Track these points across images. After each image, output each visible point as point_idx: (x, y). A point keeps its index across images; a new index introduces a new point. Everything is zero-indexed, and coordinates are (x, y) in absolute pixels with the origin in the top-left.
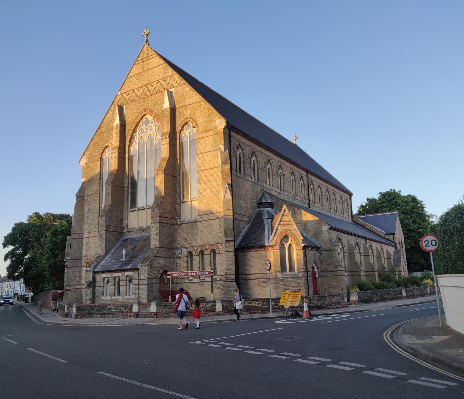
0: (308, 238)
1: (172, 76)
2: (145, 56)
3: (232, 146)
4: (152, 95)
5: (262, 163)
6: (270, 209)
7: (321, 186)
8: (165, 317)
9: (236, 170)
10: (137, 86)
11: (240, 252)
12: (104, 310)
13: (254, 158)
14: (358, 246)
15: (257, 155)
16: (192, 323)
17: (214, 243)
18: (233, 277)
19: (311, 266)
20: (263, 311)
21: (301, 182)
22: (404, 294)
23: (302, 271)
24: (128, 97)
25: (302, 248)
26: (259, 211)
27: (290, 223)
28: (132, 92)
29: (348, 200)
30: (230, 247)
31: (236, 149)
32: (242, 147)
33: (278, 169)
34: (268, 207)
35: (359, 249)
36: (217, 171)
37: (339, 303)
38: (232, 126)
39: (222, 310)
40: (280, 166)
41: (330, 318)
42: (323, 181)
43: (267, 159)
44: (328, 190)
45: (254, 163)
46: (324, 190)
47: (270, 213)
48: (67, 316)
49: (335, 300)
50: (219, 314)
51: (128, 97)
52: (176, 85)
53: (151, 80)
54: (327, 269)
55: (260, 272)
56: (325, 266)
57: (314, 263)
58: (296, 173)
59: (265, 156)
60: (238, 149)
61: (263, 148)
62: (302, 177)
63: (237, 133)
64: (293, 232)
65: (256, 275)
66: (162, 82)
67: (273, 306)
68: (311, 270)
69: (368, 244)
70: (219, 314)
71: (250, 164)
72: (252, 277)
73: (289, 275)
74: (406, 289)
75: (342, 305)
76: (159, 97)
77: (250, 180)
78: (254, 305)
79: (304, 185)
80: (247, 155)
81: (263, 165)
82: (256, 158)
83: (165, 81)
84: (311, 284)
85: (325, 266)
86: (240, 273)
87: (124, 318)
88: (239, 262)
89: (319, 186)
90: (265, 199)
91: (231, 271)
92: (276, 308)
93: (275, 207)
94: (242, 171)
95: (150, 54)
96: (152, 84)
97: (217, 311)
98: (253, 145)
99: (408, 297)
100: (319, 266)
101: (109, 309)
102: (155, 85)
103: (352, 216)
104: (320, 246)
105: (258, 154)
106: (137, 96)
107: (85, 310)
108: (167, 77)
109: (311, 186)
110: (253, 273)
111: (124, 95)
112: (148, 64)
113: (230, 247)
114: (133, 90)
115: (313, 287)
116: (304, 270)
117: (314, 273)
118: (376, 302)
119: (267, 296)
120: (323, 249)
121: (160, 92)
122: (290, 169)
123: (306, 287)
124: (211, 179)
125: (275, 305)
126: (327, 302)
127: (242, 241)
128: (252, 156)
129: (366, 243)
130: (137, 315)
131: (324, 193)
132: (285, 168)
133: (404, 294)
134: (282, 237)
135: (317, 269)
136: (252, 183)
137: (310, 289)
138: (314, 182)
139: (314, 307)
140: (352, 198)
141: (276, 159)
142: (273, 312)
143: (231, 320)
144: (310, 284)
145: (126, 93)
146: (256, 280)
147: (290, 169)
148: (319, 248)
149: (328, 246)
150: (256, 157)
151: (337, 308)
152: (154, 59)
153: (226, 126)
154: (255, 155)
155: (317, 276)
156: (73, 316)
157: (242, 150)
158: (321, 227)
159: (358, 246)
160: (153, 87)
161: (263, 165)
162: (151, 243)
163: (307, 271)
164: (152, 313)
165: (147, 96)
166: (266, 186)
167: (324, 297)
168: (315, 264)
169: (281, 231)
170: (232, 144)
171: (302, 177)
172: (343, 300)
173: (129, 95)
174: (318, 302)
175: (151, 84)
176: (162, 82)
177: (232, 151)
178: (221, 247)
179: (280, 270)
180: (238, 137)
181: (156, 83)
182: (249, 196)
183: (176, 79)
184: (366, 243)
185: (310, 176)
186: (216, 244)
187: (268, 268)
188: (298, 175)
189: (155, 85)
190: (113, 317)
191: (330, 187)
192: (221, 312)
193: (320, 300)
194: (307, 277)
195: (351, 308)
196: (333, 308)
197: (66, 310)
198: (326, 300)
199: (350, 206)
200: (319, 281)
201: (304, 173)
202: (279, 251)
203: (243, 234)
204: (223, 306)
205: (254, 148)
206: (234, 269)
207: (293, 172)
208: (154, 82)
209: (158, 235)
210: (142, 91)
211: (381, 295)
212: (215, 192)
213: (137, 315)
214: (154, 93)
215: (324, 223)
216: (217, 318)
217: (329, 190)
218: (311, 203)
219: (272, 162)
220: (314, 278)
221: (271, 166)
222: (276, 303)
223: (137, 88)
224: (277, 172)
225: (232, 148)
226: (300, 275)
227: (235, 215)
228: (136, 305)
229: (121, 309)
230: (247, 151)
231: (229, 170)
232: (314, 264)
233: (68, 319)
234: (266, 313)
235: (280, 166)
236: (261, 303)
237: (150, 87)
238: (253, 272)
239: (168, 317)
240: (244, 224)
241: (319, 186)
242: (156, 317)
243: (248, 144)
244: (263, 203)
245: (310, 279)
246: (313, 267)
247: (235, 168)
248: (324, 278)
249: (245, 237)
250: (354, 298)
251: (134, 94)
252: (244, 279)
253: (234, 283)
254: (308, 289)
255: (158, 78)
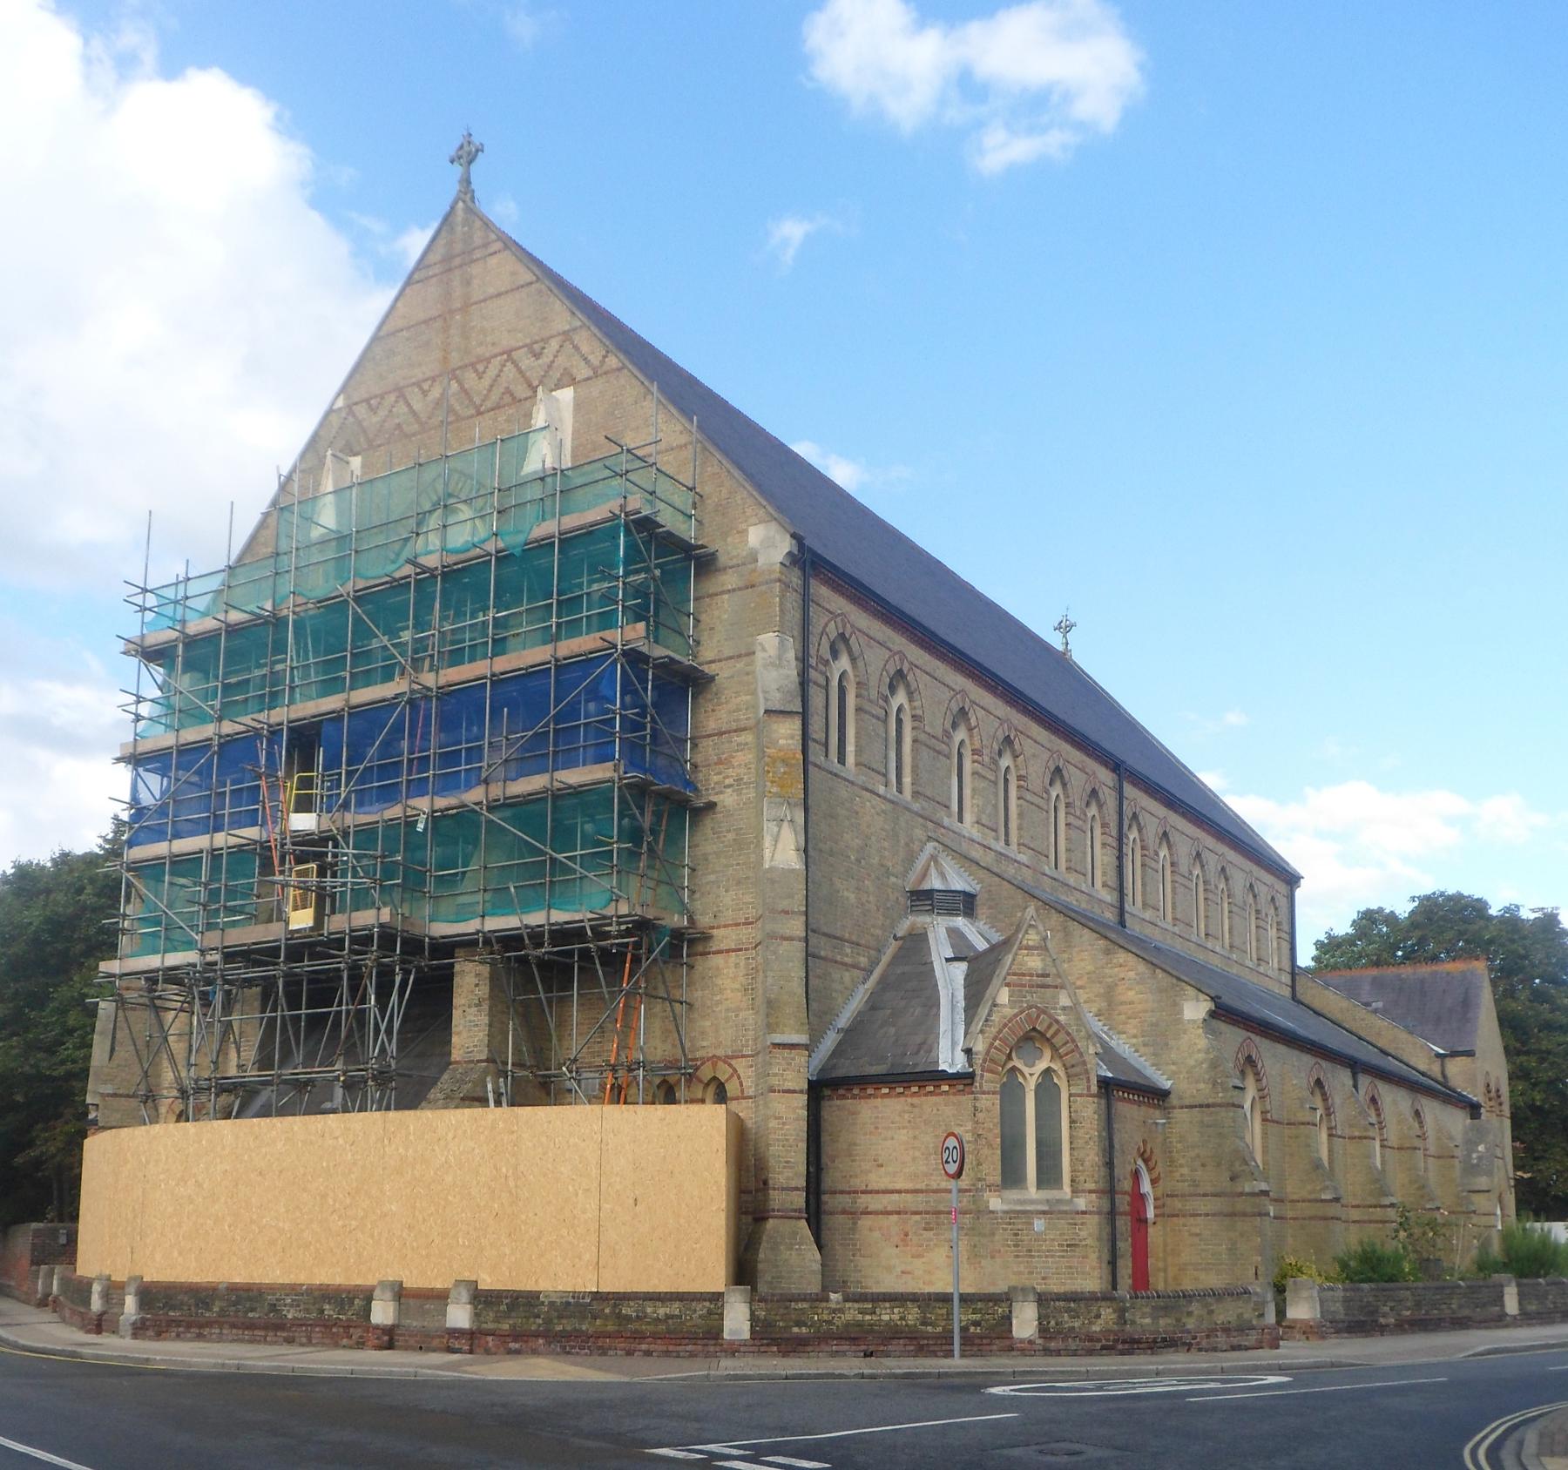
0: (1119, 1050)
1: (566, 335)
2: (458, 247)
3: (814, 639)
4: (479, 413)
5: (936, 722)
6: (960, 922)
7: (1175, 837)
8: (510, 1352)
9: (826, 745)
10: (418, 374)
11: (830, 1098)
12: (252, 1310)
13: (900, 698)
14: (1324, 1094)
15: (914, 686)
16: (626, 1379)
17: (720, 1052)
18: (799, 1199)
19: (1129, 1168)
20: (920, 1343)
21: (1093, 810)
22: (1511, 1305)
23: (1092, 1186)
24: (375, 419)
25: (1094, 1089)
26: (913, 927)
27: (1048, 981)
28: (392, 398)
29: (1282, 902)
30: (789, 1075)
31: (828, 656)
32: (855, 648)
33: (1000, 754)
34: (951, 911)
35: (1327, 1109)
36: (741, 747)
37: (1243, 1328)
38: (815, 554)
39: (747, 1335)
40: (1008, 741)
41: (1212, 1385)
42: (1184, 815)
43: (955, 708)
44: (1198, 855)
45: (899, 721)
46: (1184, 850)
47: (962, 936)
48: (99, 1325)
49: (1226, 1313)
50: (734, 1350)
51: (375, 419)
52: (583, 372)
53: (480, 351)
54: (1195, 1183)
55: (910, 1186)
56: (1185, 1171)
57: (1142, 1155)
58: (1071, 773)
59: (948, 694)
60: (835, 654)
61: (941, 657)
62: (1094, 793)
63: (837, 589)
64: (1062, 1018)
65: (895, 1197)
66: (526, 362)
67: (964, 1329)
68: (1127, 1185)
69: (1362, 1091)
70: (734, 1350)
71: (885, 721)
72: (864, 1201)
73: (1032, 1202)
74: (1518, 1285)
75: (1253, 1338)
76: (507, 421)
77: (881, 790)
78: (886, 1318)
79: (1104, 825)
80: (873, 681)
81: (939, 732)
82: (911, 700)
83: (537, 356)
84: (1124, 1246)
85: (1185, 1171)
86: (828, 1181)
87: (336, 1346)
88: (825, 1138)
89: (1165, 834)
90: (943, 876)
91: (788, 1173)
92: (976, 1336)
93: (982, 910)
94: (850, 748)
95: (477, 240)
96: (480, 368)
97: (726, 1336)
98: (899, 641)
99: (1527, 1318)
100: (1160, 1168)
101: (273, 1308)
102: (492, 372)
103: (1295, 971)
104: (1167, 1085)
105: (917, 679)
106: (414, 413)
107: (173, 1308)
108: (545, 340)
109: (1133, 835)
110: (882, 1187)
111: (361, 411)
112: (468, 283)
113: (789, 1075)
114: (400, 392)
115: (1134, 1256)
116: (1101, 1185)
117: (1138, 1198)
118: (1392, 1333)
119: (941, 1283)
120: (1181, 1098)
121: (516, 401)
122: (1046, 755)
123: (1106, 1257)
124: (716, 778)
125: (976, 1324)
126: (1191, 1324)
127: (837, 1052)
128: (892, 688)
129: (1355, 1086)
130: (389, 1339)
131: (1183, 869)
132: (1028, 747)
133: (1511, 1305)
134: (1013, 1040)
135: (1154, 1182)
136: (889, 807)
137: (1120, 1263)
138: (1144, 818)
139: (1139, 1341)
140: (1298, 893)
141: (992, 709)
142: (962, 1356)
143: (800, 1377)
144: (1120, 1244)
145: (367, 401)
146: (894, 1218)
147: (1046, 755)
148: (1163, 1095)
149: (1202, 1086)
150: (910, 694)
151: (1234, 1348)
152: (493, 261)
153: (790, 554)
154: (908, 686)
155: (1151, 1213)
156: (125, 1328)
157: (853, 660)
158: (1175, 1004)
159: (1324, 1094)
160: (486, 382)
161: (939, 732)
162: (455, 1039)
163: (1110, 1191)
164: (456, 1333)
165: (459, 419)
166: (946, 821)
167: (1182, 1302)
168: (1146, 1161)
169: (1009, 1012)
170: (816, 629)
171: (1094, 793)
172: (1262, 1315)
173: (382, 413)
174: (1155, 1318)
175: (477, 365)
176: (526, 362)
177: (813, 662)
178: (751, 1072)
179: (998, 1179)
180: (838, 603)
181: (496, 362)
182: (875, 861)
183: (585, 349)
184: (1355, 1086)
185: (1129, 790)
186: (727, 1059)
187: (952, 1168)
188: (1076, 778)
189: (492, 372)
190: (290, 1341)
191: (1210, 841)
192: (744, 1343)
193: (1166, 1310)
194: (1112, 1214)
195: (1295, 1351)
196: (1215, 1349)
197: (96, 1304)
198: (1190, 1314)
199: (1286, 927)
200: (1154, 1235)
201: (1105, 776)
202: (997, 1099)
203: (843, 1021)
204: (753, 1318)
205: (903, 657)
206: (803, 1169)
207: (1058, 770)
208: (488, 360)
209: (486, 1007)
210: (436, 393)
211: (1418, 1305)
212: (730, 836)
213: (389, 1339)
214: (489, 404)
215: (1191, 991)
216: (728, 1366)
217: (1206, 855)
218: (1127, 907)
219: (973, 722)
220: (1140, 1221)
221: (971, 736)
222: (977, 1317)
223: (418, 384)
224: (995, 763)
225: (813, 651)
226: (1081, 1203)
227: (813, 940)
228: (389, 1295)
229: (322, 1311)
230: (876, 660)
231: (796, 743)
232: (1140, 1162)
233: (107, 1340)
234: (934, 1354)
235: (1008, 741)
236: (913, 1314)
237: (470, 377)
238: (885, 1183)
239: (518, 1352)
240: (847, 976)
241: (1165, 834)
242: (471, 1352)
243: (879, 636)
244: (931, 891)
245: (1124, 1224)
246: (1136, 1175)
247: (821, 736)
248: (1181, 1221)
249: (852, 1035)
250: (1301, 1310)
251: (402, 408)
252: (844, 1212)
253: (804, 1223)
254: (1113, 1263)
255: (506, 341)
